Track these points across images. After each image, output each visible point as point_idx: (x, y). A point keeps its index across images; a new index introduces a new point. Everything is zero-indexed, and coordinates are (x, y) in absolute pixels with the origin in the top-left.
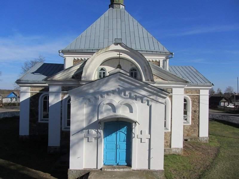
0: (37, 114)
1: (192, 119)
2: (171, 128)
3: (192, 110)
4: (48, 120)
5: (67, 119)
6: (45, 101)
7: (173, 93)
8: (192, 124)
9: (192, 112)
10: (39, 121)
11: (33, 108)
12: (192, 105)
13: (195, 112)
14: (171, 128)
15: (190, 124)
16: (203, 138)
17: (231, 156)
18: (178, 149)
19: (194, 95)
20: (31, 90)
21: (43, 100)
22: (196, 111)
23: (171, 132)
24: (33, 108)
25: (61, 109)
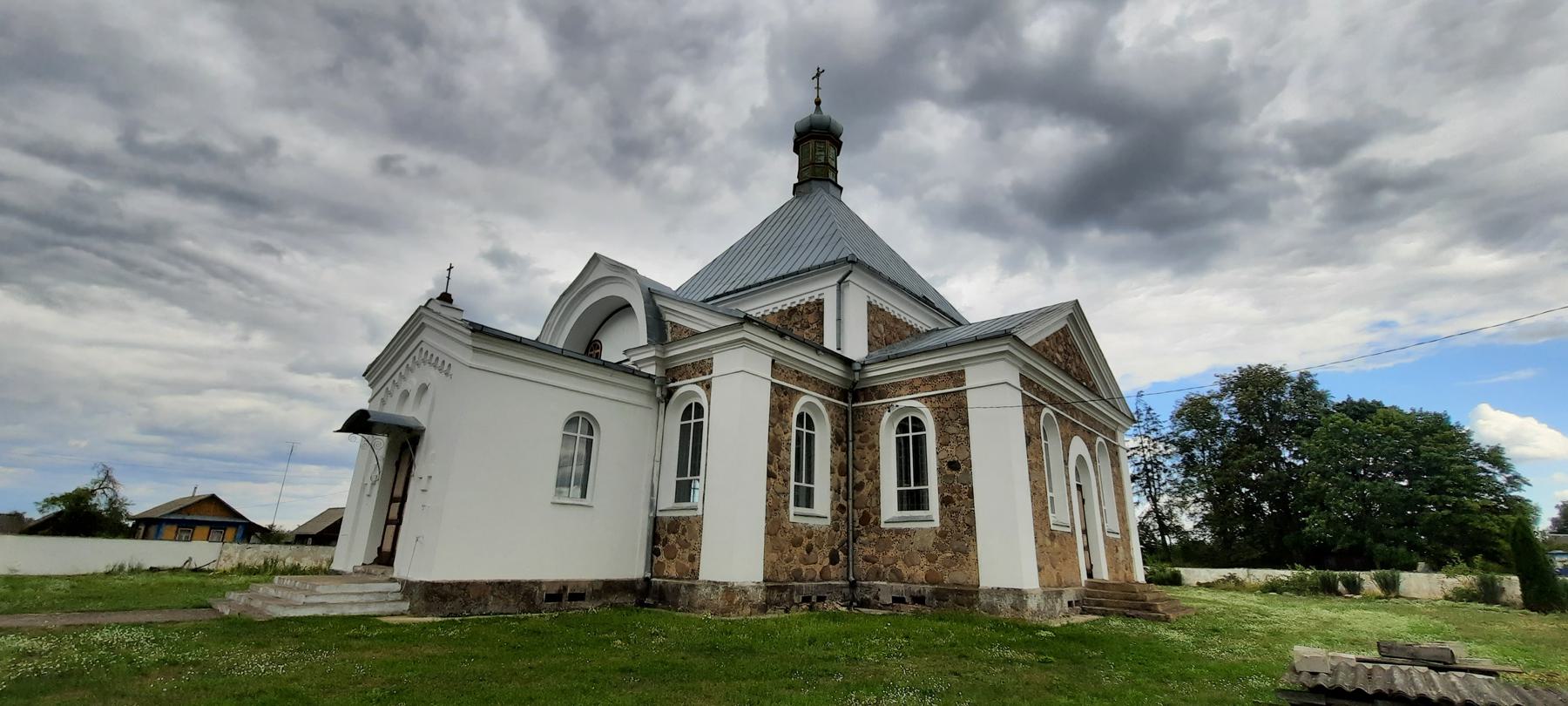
3: (940, 461)
7: (968, 384)
8: (942, 525)
9: (940, 470)
12: (938, 438)
15: (937, 524)
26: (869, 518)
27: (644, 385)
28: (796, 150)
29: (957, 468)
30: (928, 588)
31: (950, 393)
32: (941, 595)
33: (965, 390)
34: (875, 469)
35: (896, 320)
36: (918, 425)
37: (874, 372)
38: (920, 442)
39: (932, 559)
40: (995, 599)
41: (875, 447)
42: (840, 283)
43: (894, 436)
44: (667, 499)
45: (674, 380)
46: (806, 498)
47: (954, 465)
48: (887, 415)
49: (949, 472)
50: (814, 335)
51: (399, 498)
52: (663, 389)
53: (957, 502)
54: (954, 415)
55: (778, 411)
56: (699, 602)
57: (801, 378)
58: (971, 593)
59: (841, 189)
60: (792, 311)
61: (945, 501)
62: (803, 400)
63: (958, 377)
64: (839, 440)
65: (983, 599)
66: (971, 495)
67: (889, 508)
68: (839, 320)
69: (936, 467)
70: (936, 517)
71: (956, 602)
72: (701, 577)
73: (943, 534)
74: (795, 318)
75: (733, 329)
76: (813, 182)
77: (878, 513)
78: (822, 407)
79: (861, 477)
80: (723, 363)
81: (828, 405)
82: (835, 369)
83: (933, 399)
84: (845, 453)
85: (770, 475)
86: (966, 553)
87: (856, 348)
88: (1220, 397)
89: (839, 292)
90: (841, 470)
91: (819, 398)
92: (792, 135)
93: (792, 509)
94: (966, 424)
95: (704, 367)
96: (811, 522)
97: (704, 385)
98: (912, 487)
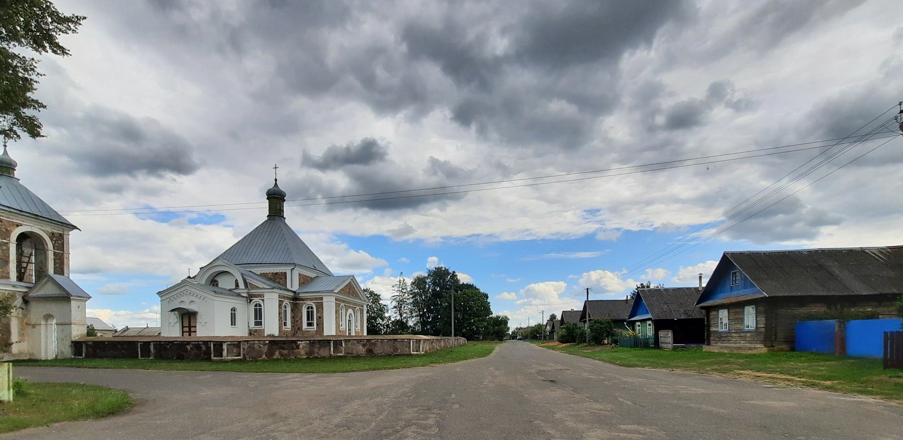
3: (317, 317)
7: (324, 300)
9: (317, 318)
26: (300, 328)
27: (245, 299)
29: (320, 318)
34: (301, 317)
35: (306, 276)
36: (312, 308)
37: (301, 295)
38: (312, 312)
41: (301, 312)
42: (291, 270)
43: (306, 310)
44: (252, 325)
45: (252, 297)
46: (285, 324)
47: (320, 318)
48: (304, 305)
50: (283, 282)
52: (250, 298)
54: (320, 307)
55: (280, 306)
57: (284, 297)
59: (285, 218)
60: (276, 273)
61: (317, 325)
62: (285, 302)
63: (322, 299)
64: (292, 310)
67: (305, 326)
68: (291, 279)
70: (316, 328)
74: (277, 276)
76: (276, 217)
77: (302, 327)
78: (289, 303)
79: (298, 319)
80: (267, 296)
81: (290, 303)
82: (292, 294)
85: (279, 320)
87: (296, 287)
88: (427, 278)
89: (291, 271)
90: (293, 317)
91: (260, 288)
93: (283, 327)
94: (323, 309)
95: (261, 296)
96: (287, 329)
98: (258, 320)
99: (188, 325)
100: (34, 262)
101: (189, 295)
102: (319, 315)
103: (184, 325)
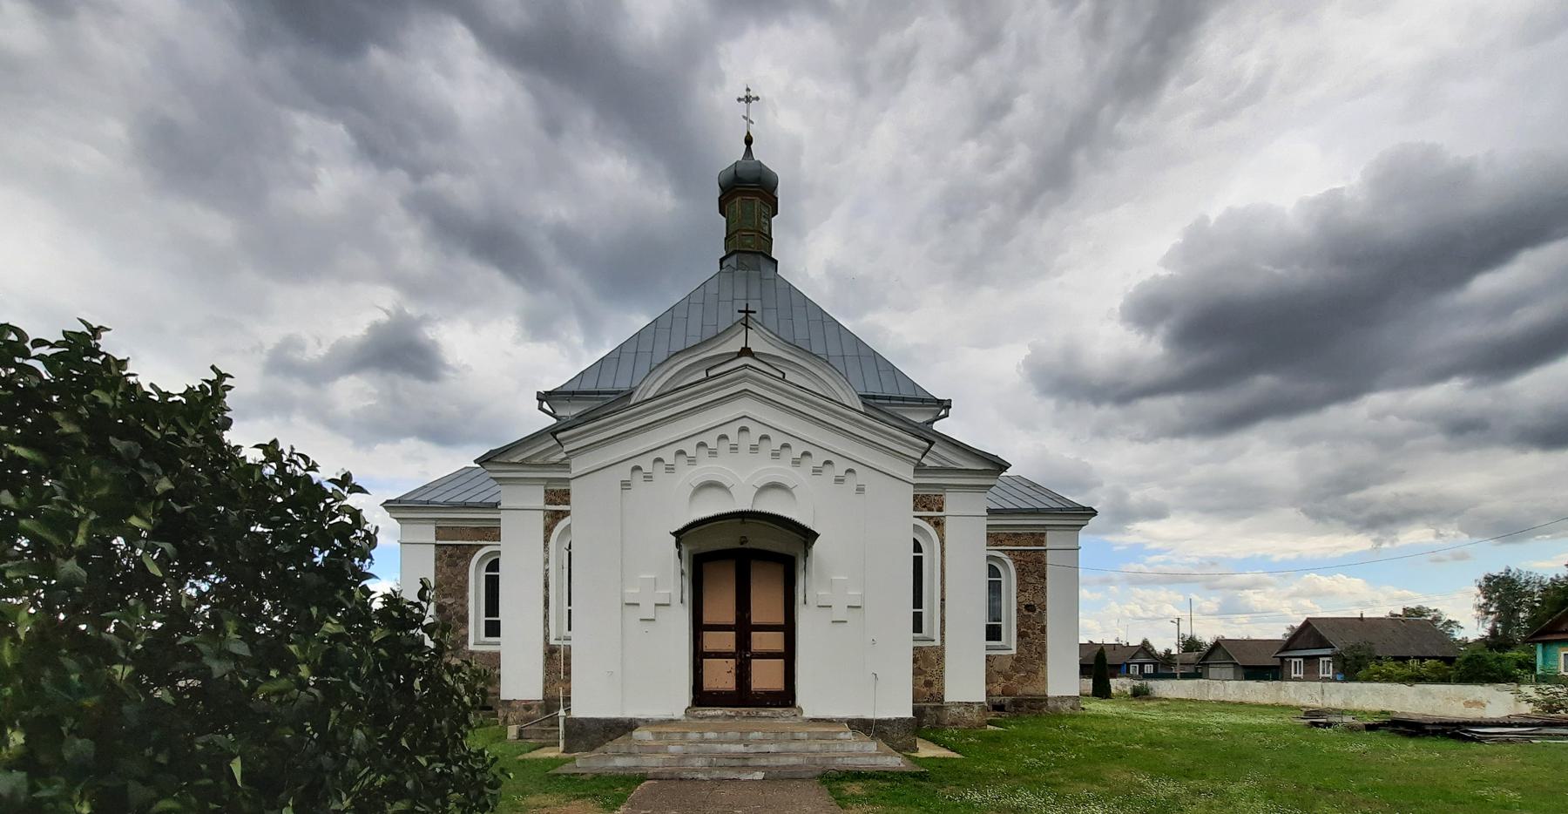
0: (464, 620)
1: (1021, 635)
2: (942, 634)
3: (1019, 603)
4: (499, 644)
5: (925, 610)
6: (918, 608)
7: (947, 510)
8: (1018, 653)
9: (1018, 610)
10: (471, 647)
11: (449, 601)
12: (1018, 585)
13: (1029, 611)
14: (942, 634)
15: (1014, 652)
16: (1062, 699)
17: (1122, 734)
18: (969, 705)
19: (1025, 550)
20: (991, 619)
21: (483, 573)
22: (1031, 605)
23: (942, 648)
24: (449, 601)
25: (570, 604)
28: (722, 211)
30: (1008, 699)
31: (1030, 550)
32: (1017, 704)
33: (1046, 550)
39: (1008, 678)
40: (1059, 703)
47: (1030, 608)
49: (1026, 613)
51: (732, 625)
53: (1031, 636)
56: (949, 719)
58: (1041, 701)
63: (1039, 539)
65: (1050, 704)
66: (1043, 630)
69: (1016, 608)
70: (1014, 646)
71: (1030, 707)
72: (947, 699)
73: (1018, 659)
75: (978, 474)
83: (1016, 553)
84: (1471, 626)
86: (1036, 673)
92: (717, 192)
97: (932, 521)
99: (731, 619)
100: (924, 461)
101: (754, 449)
102: (1028, 597)
103: (708, 619)
